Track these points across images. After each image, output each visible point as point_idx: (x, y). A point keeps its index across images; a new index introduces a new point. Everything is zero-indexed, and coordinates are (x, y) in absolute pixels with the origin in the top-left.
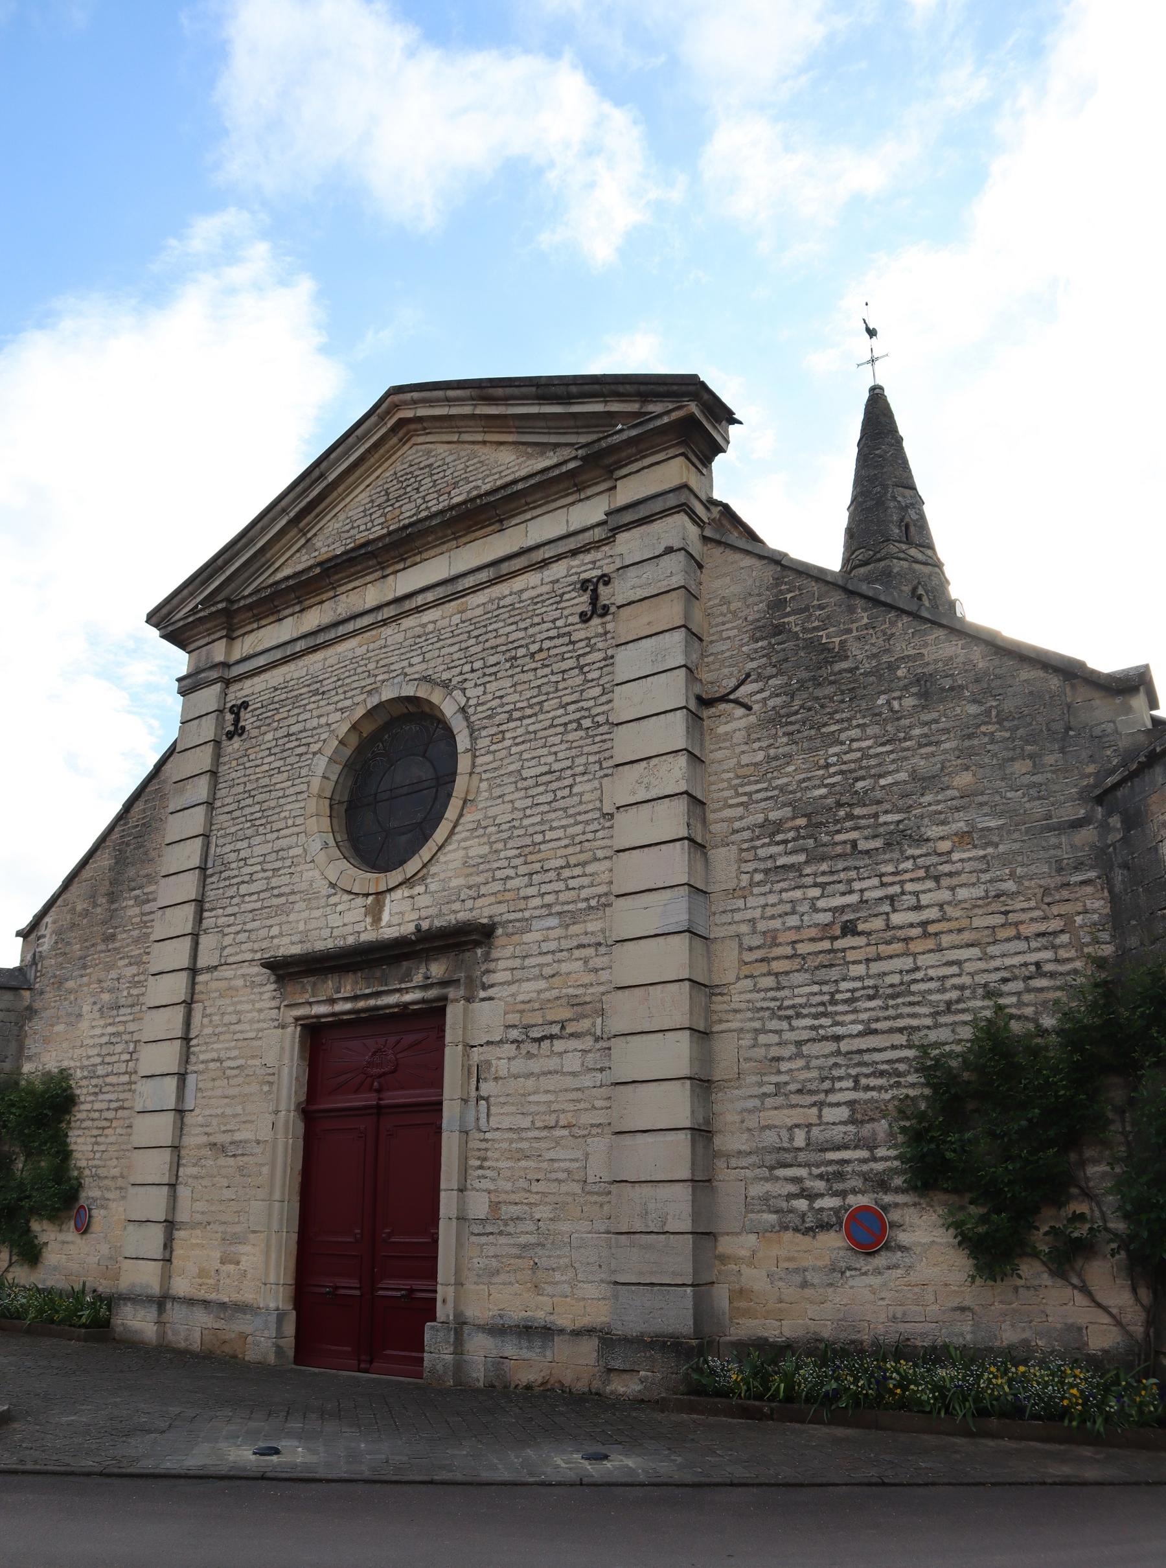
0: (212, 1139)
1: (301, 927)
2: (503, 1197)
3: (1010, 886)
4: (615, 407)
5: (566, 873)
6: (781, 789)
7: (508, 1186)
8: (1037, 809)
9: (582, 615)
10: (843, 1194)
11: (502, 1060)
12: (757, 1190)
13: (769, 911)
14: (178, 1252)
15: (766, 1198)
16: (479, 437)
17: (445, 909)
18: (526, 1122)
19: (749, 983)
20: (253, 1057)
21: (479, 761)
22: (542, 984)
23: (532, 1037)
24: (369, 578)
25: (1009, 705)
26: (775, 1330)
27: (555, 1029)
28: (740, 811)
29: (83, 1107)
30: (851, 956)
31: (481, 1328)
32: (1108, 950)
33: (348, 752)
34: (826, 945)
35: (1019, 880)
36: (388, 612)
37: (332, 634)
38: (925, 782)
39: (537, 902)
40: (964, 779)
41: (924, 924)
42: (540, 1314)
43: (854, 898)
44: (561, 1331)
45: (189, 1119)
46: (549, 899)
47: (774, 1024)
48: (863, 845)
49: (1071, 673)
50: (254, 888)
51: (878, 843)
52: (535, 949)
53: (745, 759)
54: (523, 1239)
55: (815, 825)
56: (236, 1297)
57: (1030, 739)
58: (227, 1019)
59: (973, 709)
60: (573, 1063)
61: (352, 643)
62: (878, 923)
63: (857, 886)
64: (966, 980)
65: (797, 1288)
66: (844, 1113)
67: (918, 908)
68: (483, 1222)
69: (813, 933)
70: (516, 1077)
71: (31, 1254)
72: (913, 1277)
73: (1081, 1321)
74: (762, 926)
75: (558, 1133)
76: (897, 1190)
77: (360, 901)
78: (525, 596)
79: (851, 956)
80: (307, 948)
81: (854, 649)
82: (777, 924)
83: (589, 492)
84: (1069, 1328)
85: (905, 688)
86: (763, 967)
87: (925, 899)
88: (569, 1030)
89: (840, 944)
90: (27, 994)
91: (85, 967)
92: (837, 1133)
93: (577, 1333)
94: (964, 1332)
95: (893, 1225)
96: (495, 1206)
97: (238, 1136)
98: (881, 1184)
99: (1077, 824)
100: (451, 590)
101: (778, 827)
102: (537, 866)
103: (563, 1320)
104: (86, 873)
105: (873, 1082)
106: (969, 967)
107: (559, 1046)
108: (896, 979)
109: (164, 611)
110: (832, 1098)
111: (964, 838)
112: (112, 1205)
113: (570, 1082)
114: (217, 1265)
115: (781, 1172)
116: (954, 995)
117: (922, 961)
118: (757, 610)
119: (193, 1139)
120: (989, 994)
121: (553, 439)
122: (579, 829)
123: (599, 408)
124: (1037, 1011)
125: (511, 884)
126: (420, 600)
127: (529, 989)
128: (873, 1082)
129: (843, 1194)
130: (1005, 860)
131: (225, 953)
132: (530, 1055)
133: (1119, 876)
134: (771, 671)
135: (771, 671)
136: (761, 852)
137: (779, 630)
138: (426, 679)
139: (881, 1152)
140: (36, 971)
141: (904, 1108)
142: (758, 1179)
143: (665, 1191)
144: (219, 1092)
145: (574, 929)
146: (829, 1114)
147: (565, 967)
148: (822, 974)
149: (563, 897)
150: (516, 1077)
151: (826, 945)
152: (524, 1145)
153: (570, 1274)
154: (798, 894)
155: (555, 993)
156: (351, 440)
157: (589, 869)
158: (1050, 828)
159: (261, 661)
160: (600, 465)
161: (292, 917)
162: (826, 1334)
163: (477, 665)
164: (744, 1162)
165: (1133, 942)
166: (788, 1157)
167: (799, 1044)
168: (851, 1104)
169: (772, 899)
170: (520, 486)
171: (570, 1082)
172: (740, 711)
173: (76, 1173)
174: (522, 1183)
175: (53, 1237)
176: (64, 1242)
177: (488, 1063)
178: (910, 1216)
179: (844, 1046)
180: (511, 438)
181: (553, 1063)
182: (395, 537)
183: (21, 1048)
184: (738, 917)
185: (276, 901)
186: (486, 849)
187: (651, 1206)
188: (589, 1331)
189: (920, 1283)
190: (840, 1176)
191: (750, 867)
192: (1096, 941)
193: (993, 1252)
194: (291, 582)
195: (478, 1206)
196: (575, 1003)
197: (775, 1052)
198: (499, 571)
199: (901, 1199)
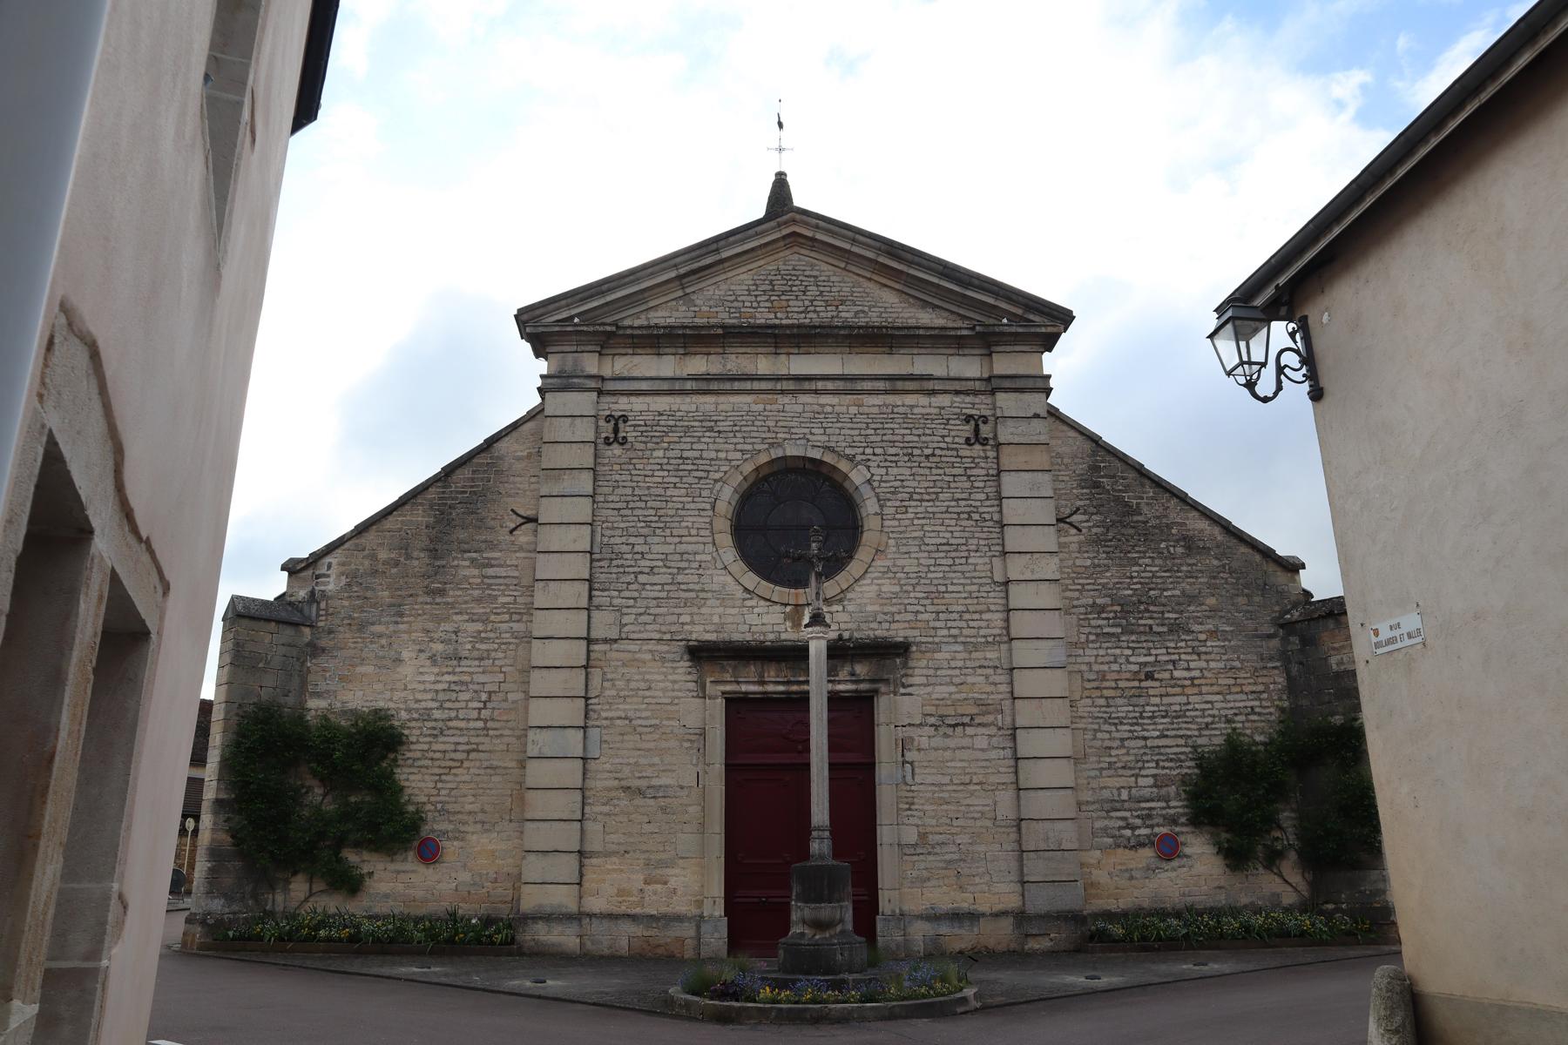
0: (624, 783)
1: (716, 619)
2: (929, 829)
3: (1237, 664)
4: (1004, 305)
5: (967, 616)
6: (1104, 585)
7: (934, 822)
8: (1250, 624)
9: (968, 439)
10: (1152, 827)
11: (923, 737)
12: (1099, 824)
13: (1100, 660)
14: (589, 876)
15: (1105, 829)
16: (868, 275)
17: (863, 626)
18: (946, 780)
19: (1089, 701)
20: (669, 719)
21: (887, 523)
22: (953, 689)
23: (948, 723)
24: (760, 350)
25: (1235, 565)
26: (1112, 905)
27: (966, 720)
28: (1076, 594)
29: (413, 747)
30: (1151, 692)
31: (921, 917)
32: (1286, 704)
33: (746, 486)
34: (1136, 684)
35: (1242, 662)
36: (786, 385)
37: (728, 386)
38: (1192, 599)
39: (945, 632)
40: (1212, 601)
41: (1192, 679)
42: (965, 905)
43: (1152, 659)
44: (983, 915)
45: (592, 765)
46: (953, 632)
47: (1106, 727)
48: (1156, 629)
49: (1267, 553)
50: (655, 579)
51: (1165, 629)
52: (945, 664)
53: (1078, 562)
54: (948, 857)
55: (1125, 613)
56: (663, 909)
57: (1246, 586)
58: (633, 685)
59: (1216, 562)
60: (981, 742)
61: (749, 399)
62: (1167, 675)
63: (1153, 652)
64: (1215, 712)
65: (1132, 882)
66: (1150, 781)
67: (1188, 669)
68: (915, 846)
69: (1128, 675)
70: (936, 749)
71: (351, 884)
72: (1194, 871)
73: (1279, 891)
74: (1096, 667)
75: (972, 787)
76: (1183, 825)
77: (778, 608)
78: (916, 411)
79: (1151, 692)
80: (724, 636)
81: (1145, 510)
82: (1105, 667)
83: (966, 351)
84: (1273, 894)
85: (1177, 541)
86: (1098, 693)
87: (1192, 665)
88: (977, 721)
89: (1144, 684)
90: (307, 631)
91: (401, 615)
92: (1146, 792)
93: (997, 915)
94: (1221, 899)
95: (1184, 844)
96: (923, 836)
97: (655, 782)
98: (1173, 821)
99: (1270, 636)
100: (849, 384)
101: (1102, 609)
102: (943, 608)
103: (983, 907)
104: (389, 524)
105: (1167, 764)
106: (1218, 705)
107: (969, 731)
108: (1177, 708)
109: (538, 312)
110: (1143, 772)
111: (1213, 634)
112: (469, 837)
113: (980, 755)
114: (641, 885)
115: (1114, 814)
116: (1209, 720)
117: (1191, 699)
118: (1082, 468)
119: (598, 783)
120: (1229, 721)
121: (962, 312)
122: (975, 588)
123: (991, 301)
124: (1258, 731)
125: (920, 617)
126: (820, 385)
127: (941, 691)
128: (1167, 764)
129: (1152, 827)
130: (1235, 649)
131: (626, 629)
132: (946, 735)
133: (1295, 669)
134: (1092, 510)
135: (1092, 510)
136: (1093, 623)
137: (1097, 485)
138: (831, 450)
139: (1173, 804)
140: (318, 609)
141: (1184, 779)
142: (1099, 818)
143: (1059, 825)
144: (631, 745)
145: (974, 655)
146: (1141, 781)
147: (970, 679)
148: (1134, 700)
149: (965, 632)
150: (936, 749)
151: (1136, 684)
152: (946, 795)
153: (987, 878)
154: (1118, 651)
155: (964, 695)
156: (751, 232)
157: (985, 616)
158: (1257, 636)
159: (644, 386)
160: (987, 341)
161: (703, 610)
162: (1145, 905)
163: (878, 451)
164: (1091, 808)
165: (1305, 702)
166: (1118, 805)
167: (1122, 740)
168: (1154, 776)
169: (1102, 652)
170: (921, 332)
171: (980, 755)
172: (1074, 531)
173: (411, 808)
174: (944, 820)
175: (380, 866)
176: (398, 872)
177: (912, 739)
178: (1190, 839)
179: (1149, 743)
180: (897, 286)
181: (966, 742)
182: (804, 331)
183: (304, 683)
184: (1079, 660)
185: (683, 595)
186: (897, 589)
187: (1051, 834)
188: (1004, 913)
189: (1198, 874)
190: (1149, 816)
191: (1087, 630)
192: (1280, 699)
193: (1235, 858)
194: (688, 332)
195: (911, 836)
196: (978, 703)
197: (1107, 743)
198: (895, 383)
199: (1184, 829)
